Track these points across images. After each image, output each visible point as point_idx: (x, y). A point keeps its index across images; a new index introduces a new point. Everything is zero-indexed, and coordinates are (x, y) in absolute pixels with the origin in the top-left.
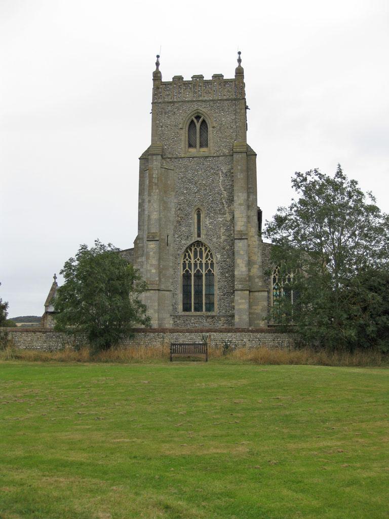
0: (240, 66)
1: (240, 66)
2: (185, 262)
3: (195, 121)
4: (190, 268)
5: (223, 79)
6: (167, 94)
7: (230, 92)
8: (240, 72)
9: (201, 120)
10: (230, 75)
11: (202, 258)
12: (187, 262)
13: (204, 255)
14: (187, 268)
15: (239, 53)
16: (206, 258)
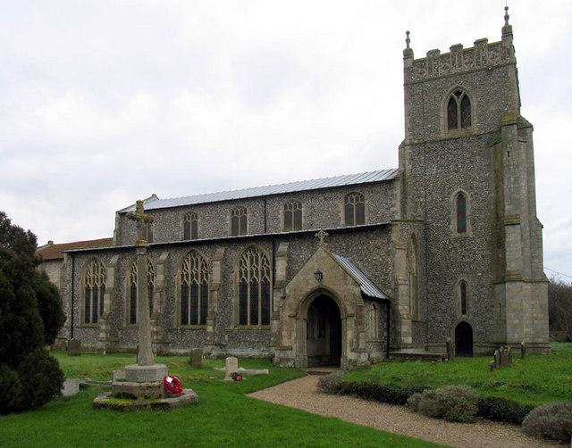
0: (408, 46)
1: (507, 23)
3: (455, 97)
6: (424, 75)
8: (507, 32)
10: (495, 37)
11: (257, 264)
13: (260, 261)
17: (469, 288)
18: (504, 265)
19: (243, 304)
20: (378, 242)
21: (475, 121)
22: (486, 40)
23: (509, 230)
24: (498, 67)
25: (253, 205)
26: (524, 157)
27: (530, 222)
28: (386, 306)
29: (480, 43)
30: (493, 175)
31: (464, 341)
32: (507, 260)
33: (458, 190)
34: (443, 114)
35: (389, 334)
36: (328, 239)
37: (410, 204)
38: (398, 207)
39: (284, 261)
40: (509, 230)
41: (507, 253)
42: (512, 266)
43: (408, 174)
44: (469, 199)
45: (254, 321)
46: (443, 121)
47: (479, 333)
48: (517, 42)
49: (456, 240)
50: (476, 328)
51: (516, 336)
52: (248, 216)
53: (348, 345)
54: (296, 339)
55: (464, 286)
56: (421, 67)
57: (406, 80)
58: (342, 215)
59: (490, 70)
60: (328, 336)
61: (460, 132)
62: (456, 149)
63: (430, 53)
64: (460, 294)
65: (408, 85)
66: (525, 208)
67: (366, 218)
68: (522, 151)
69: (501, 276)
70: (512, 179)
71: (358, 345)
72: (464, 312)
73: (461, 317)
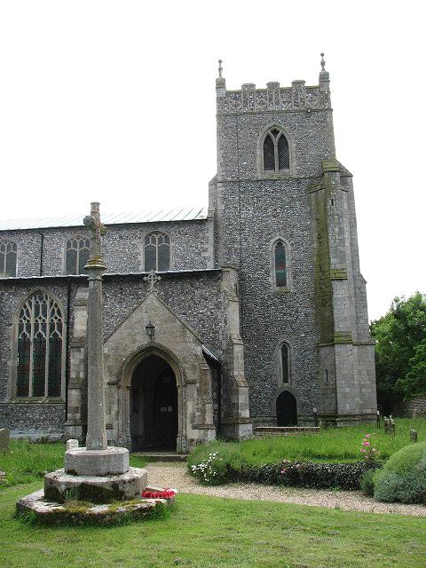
0: (323, 69)
2: (21, 321)
4: (44, 330)
5: (310, 89)
6: (237, 109)
7: (311, 104)
8: (324, 78)
9: (279, 135)
11: (46, 316)
12: (40, 322)
14: (25, 331)
15: (220, 62)
16: (35, 317)
17: (291, 352)
18: (332, 324)
19: (23, 369)
20: (206, 292)
21: (293, 164)
22: (303, 82)
23: (336, 285)
24: (317, 111)
25: (26, 239)
26: (346, 207)
27: (354, 278)
28: (218, 369)
29: (298, 84)
30: (314, 224)
31: (286, 412)
32: (336, 320)
33: (277, 238)
34: (260, 152)
35: (220, 406)
36: (161, 284)
37: (223, 250)
38: (210, 253)
39: (85, 313)
40: (336, 285)
41: (335, 311)
42: (340, 327)
43: (220, 213)
44: (288, 248)
45: (39, 392)
46: (260, 160)
47: (304, 405)
48: (332, 86)
49: (276, 294)
50: (300, 399)
51: (348, 407)
52: (19, 252)
53: (188, 421)
54: (118, 413)
55: (285, 350)
56: (236, 99)
57: (218, 111)
58: (141, 258)
59: (309, 113)
60: (141, 410)
61: (275, 174)
62: (275, 191)
63: (245, 86)
64: (281, 359)
65: (221, 117)
66: (349, 257)
67: (172, 264)
68: (344, 200)
69: (327, 335)
70: (337, 230)
71: (205, 419)
72: (285, 380)
73: (282, 386)
